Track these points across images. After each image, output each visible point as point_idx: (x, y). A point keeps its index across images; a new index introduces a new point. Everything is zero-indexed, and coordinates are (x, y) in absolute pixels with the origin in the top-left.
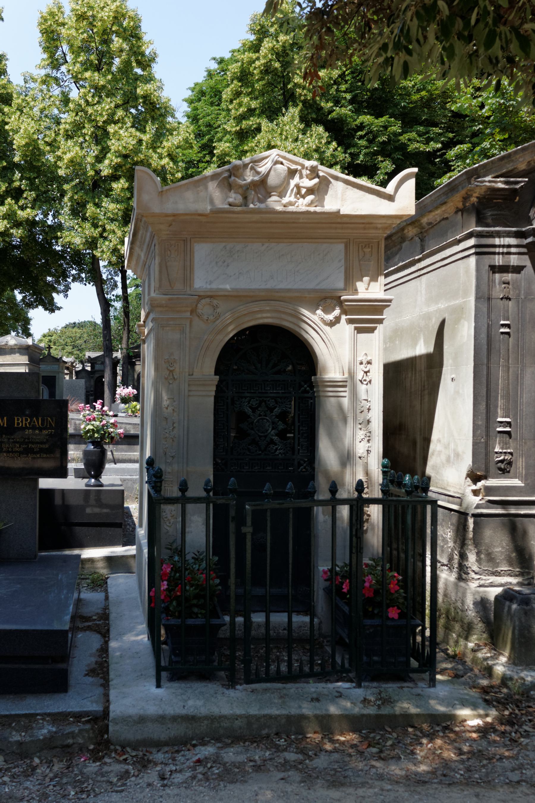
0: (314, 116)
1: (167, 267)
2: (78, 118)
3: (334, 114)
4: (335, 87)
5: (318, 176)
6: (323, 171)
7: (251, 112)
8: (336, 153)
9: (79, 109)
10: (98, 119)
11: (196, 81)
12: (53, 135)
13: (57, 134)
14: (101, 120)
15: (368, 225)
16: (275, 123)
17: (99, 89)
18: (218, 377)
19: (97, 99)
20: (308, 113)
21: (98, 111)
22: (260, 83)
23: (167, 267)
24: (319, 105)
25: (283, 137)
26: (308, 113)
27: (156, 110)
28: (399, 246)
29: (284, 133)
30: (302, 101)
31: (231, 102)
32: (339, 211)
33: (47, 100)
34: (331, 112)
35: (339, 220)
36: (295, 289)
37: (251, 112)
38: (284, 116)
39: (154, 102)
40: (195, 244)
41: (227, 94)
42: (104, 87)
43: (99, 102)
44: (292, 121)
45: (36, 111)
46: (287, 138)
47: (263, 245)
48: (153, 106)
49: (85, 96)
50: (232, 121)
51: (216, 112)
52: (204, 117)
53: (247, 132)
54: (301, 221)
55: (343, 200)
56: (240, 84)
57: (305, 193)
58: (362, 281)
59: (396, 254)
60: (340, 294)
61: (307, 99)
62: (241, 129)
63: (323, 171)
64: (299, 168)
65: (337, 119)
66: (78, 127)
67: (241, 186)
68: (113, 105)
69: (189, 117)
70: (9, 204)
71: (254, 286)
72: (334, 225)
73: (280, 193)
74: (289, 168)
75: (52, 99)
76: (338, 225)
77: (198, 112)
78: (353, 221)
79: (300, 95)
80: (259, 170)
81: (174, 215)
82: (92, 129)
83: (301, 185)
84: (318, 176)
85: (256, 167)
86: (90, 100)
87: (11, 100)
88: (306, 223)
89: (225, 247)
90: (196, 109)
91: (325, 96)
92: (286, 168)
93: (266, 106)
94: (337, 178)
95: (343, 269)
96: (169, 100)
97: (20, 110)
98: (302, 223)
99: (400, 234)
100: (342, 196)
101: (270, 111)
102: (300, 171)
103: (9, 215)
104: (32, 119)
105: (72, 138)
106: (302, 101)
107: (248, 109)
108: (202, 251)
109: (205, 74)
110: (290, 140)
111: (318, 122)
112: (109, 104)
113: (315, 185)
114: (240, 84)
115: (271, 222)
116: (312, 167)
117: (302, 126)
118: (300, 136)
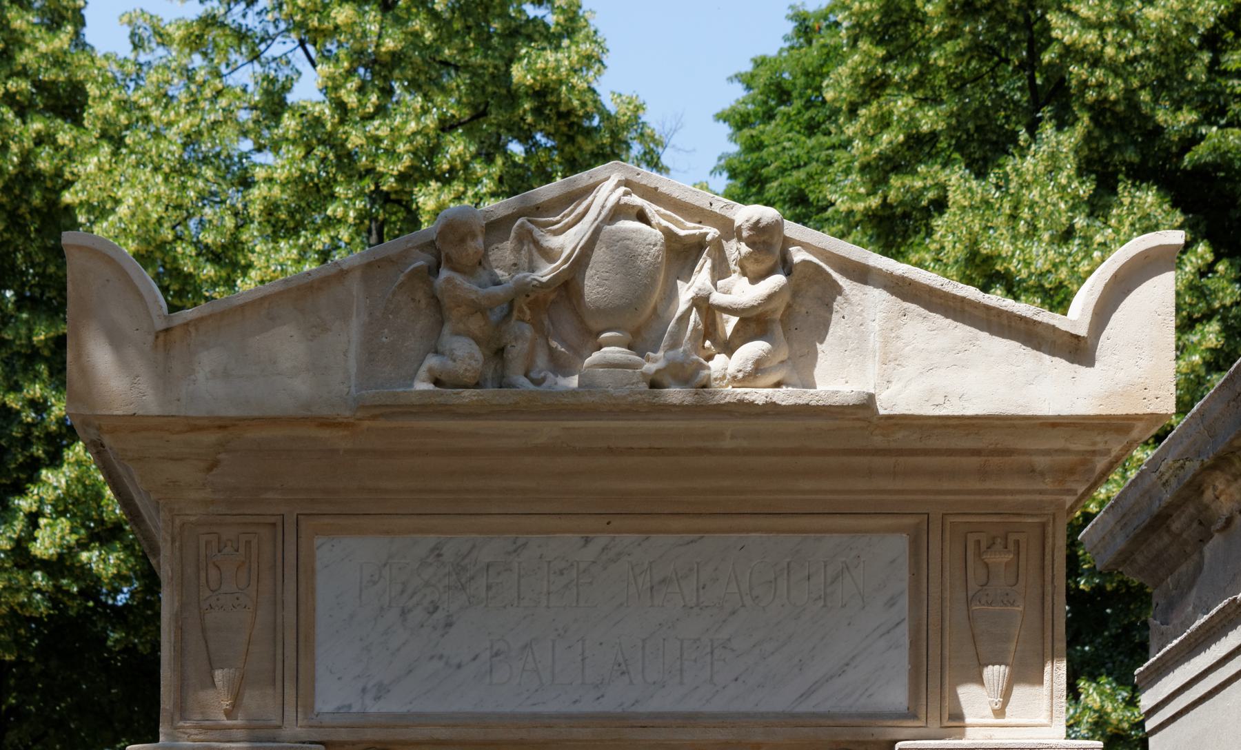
0: (1132, 156)
1: (204, 630)
2: (312, 167)
3: (1201, 152)
4: (1206, 57)
5: (786, 266)
6: (805, 246)
7: (920, 146)
8: (1211, 283)
9: (313, 133)
10: (381, 166)
11: (759, 52)
12: (230, 223)
13: (243, 220)
14: (390, 169)
15: (996, 460)
16: (992, 178)
17: (384, 65)
19: (374, 98)
20: (1112, 148)
21: (378, 140)
22: (949, 46)
23: (204, 630)
24: (1151, 118)
25: (1022, 227)
26: (1112, 148)
27: (580, 139)
28: (1196, 557)
29: (1025, 213)
30: (1090, 108)
31: (853, 112)
32: (869, 403)
33: (206, 105)
34: (1191, 140)
35: (878, 441)
36: (714, 716)
37: (920, 146)
38: (1023, 157)
39: (570, 112)
40: (318, 541)
41: (838, 86)
42: (397, 58)
43: (381, 111)
44: (1053, 169)
45: (172, 147)
46: (1032, 231)
47: (587, 541)
48: (571, 125)
49: (336, 88)
50: (855, 177)
51: (823, 154)
52: (783, 171)
53: (906, 215)
54: (728, 444)
55: (890, 359)
56: (881, 52)
57: (736, 330)
58: (979, 680)
59: (1190, 587)
60: (891, 734)
61: (1106, 99)
62: (885, 204)
63: (805, 246)
64: (712, 232)
65: (1216, 167)
66: (311, 193)
67: (478, 309)
68: (430, 121)
69: (733, 175)
70: (79, 463)
71: (554, 704)
72: (863, 461)
73: (636, 333)
74: (668, 234)
75: (223, 102)
76: (878, 461)
77: (764, 153)
78: (933, 443)
79: (1084, 85)
80: (553, 242)
81: (223, 425)
82: (359, 204)
83: (717, 298)
84: (786, 266)
85: (537, 232)
86: (352, 100)
87: (83, 105)
88: (747, 452)
89: (437, 551)
90: (755, 146)
91: (1170, 90)
92: (658, 235)
93: (971, 126)
94: (862, 274)
95: (903, 635)
96: (637, 108)
97: (110, 139)
98: (734, 452)
99: (1191, 509)
100: (886, 342)
101: (982, 143)
102: (718, 245)
103: (76, 502)
104: (156, 169)
105: (294, 232)
106: (1090, 108)
107: (908, 137)
108: (344, 566)
109: (789, 27)
110: (1046, 236)
111: (1140, 175)
112: (418, 118)
113: (771, 297)
114: (881, 52)
115: (610, 451)
116: (756, 227)
117: (1085, 189)
118: (1080, 222)
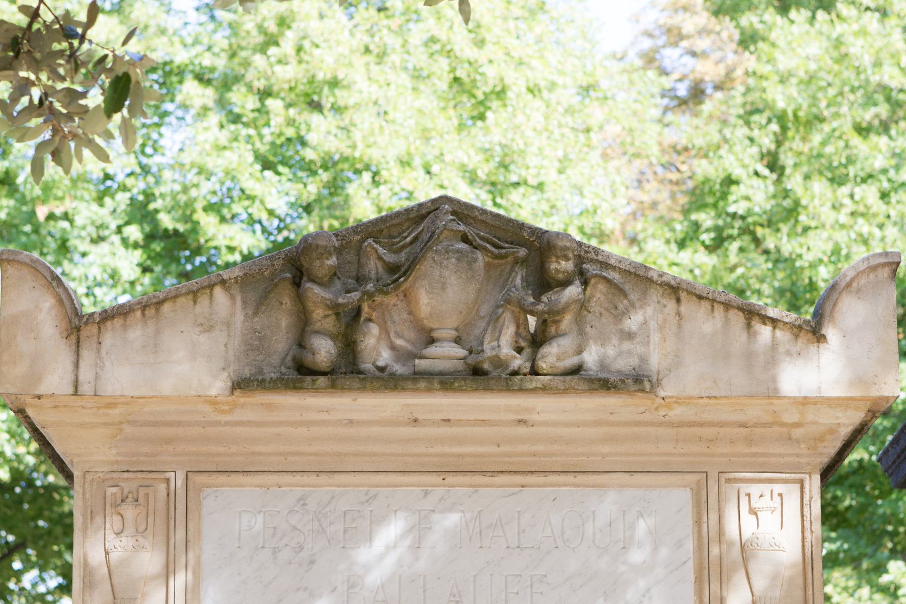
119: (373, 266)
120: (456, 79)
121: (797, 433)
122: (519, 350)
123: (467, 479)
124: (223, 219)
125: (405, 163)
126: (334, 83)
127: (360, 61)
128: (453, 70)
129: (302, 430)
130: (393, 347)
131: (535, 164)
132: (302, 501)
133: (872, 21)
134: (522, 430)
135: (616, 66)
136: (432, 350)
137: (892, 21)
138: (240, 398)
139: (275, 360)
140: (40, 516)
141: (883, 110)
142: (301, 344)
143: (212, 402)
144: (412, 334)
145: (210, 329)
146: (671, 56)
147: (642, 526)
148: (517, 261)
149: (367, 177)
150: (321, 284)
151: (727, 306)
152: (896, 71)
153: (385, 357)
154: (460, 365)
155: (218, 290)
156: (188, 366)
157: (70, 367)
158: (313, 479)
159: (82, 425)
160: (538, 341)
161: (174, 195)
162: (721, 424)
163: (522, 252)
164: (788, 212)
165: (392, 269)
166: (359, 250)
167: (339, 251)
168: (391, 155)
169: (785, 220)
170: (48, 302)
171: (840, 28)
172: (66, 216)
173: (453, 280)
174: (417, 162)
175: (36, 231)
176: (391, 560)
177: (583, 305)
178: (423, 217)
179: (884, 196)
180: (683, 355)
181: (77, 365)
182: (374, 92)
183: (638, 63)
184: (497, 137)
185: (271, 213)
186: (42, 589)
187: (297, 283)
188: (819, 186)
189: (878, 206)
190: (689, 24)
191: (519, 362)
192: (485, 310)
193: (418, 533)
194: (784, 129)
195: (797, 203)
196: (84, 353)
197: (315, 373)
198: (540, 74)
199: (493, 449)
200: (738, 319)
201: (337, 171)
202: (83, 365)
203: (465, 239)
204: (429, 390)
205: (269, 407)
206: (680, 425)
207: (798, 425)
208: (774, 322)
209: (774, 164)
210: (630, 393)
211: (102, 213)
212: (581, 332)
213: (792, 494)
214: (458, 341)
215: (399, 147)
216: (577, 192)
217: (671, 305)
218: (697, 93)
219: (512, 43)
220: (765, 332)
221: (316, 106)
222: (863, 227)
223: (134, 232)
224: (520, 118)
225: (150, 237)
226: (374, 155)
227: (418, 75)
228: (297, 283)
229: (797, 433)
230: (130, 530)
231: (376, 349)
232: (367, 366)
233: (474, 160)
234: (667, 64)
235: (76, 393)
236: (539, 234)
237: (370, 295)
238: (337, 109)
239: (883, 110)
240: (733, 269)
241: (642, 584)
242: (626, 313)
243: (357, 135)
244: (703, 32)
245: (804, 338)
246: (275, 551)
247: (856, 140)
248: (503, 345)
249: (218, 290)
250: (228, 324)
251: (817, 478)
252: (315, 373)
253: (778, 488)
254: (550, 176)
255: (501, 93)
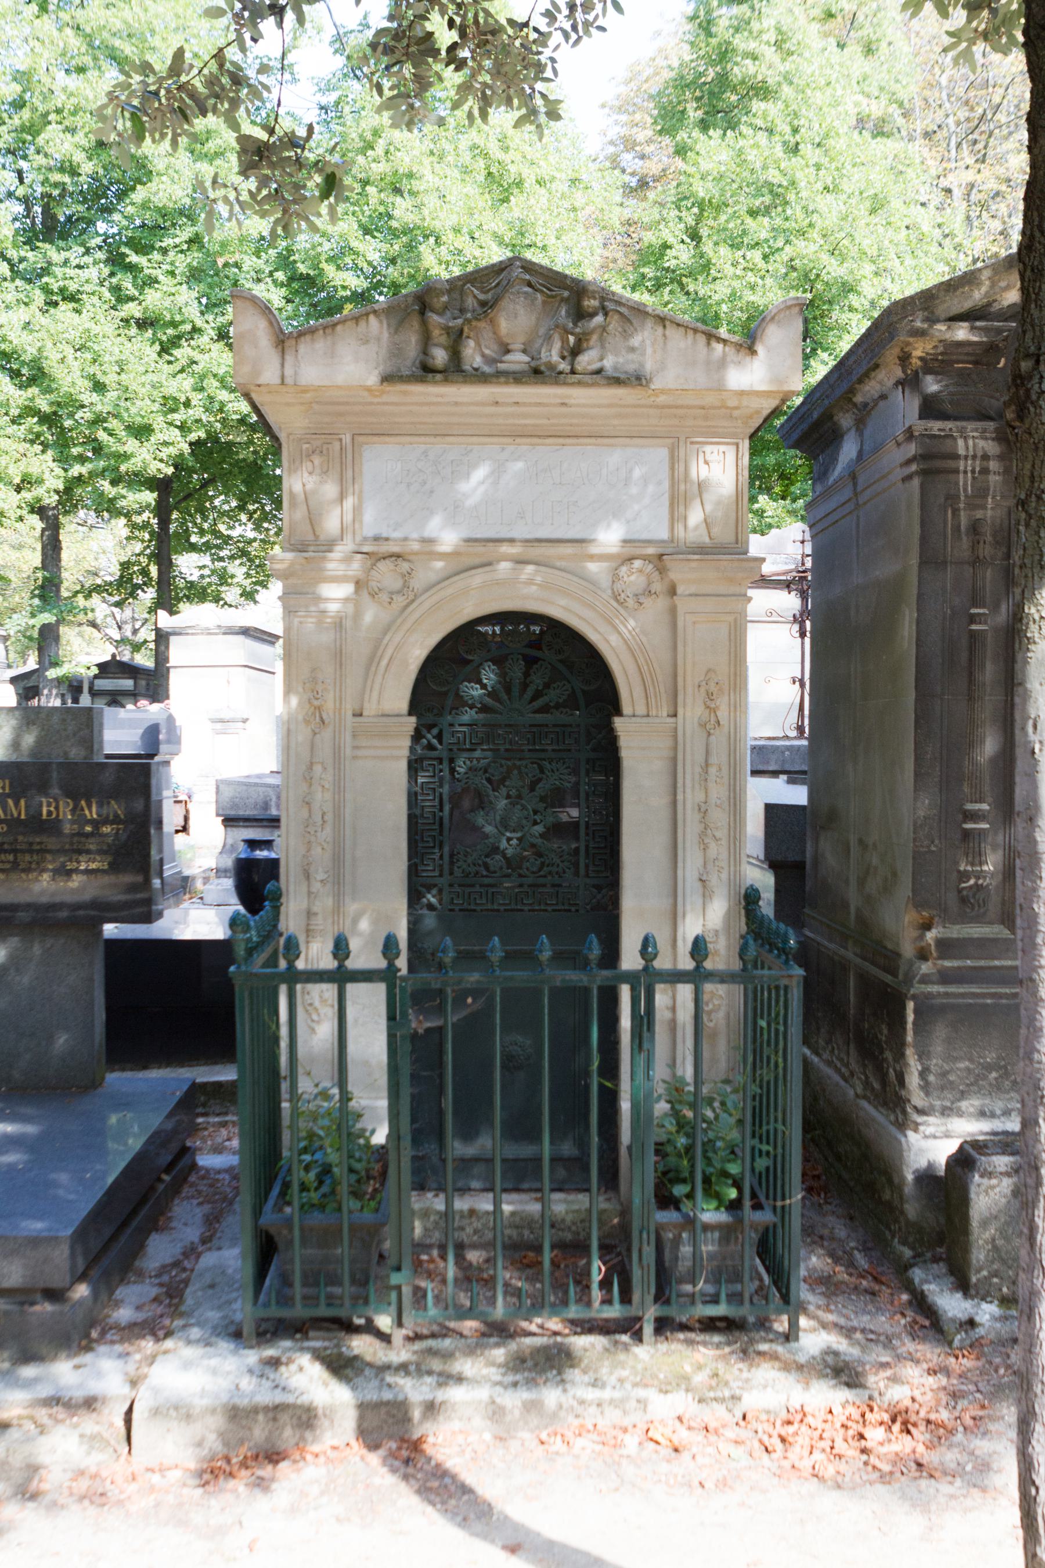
18: (413, 719)
119: (470, 302)
120: (489, 174)
121: (736, 413)
122: (563, 358)
123: (528, 440)
124: (339, 268)
125: (457, 231)
126: (410, 175)
127: (427, 161)
128: (488, 167)
129: (425, 408)
130: (483, 355)
131: (543, 232)
132: (425, 453)
133: (762, 137)
134: (564, 409)
135: (593, 166)
136: (509, 357)
137: (777, 138)
138: (387, 387)
139: (409, 363)
140: (224, 461)
141: (767, 199)
142: (425, 352)
143: (368, 389)
144: (495, 347)
145: (367, 342)
146: (628, 159)
147: (637, 473)
148: (563, 300)
149: (432, 240)
150: (440, 314)
151: (695, 331)
152: (777, 173)
153: (478, 361)
154: (526, 367)
155: (372, 317)
156: (350, 364)
157: (278, 366)
158: (432, 439)
159: (288, 404)
160: (575, 352)
161: (307, 252)
162: (689, 407)
163: (566, 294)
164: (704, 267)
165: (483, 304)
166: (462, 292)
167: (449, 292)
168: (449, 224)
169: (700, 273)
170: (262, 324)
171: (742, 142)
172: (237, 265)
173: (522, 312)
174: (465, 230)
175: (217, 274)
176: (482, 489)
177: (604, 328)
178: (503, 270)
179: (765, 257)
180: (669, 363)
181: (283, 365)
182: (437, 182)
183: (608, 164)
184: (517, 213)
185: (370, 263)
186: (226, 507)
187: (422, 313)
188: (724, 250)
189: (761, 264)
190: (642, 135)
191: (564, 366)
192: (542, 331)
193: (498, 472)
194: (702, 210)
195: (709, 261)
196: (287, 357)
197: (433, 371)
198: (545, 171)
199: (545, 421)
200: (702, 339)
201: (412, 237)
202: (287, 366)
203: (530, 285)
204: (507, 383)
205: (405, 393)
206: (663, 407)
207: (737, 408)
208: (725, 341)
209: (695, 236)
210: (633, 386)
211: (260, 263)
212: (603, 347)
213: (731, 452)
214: (524, 351)
215: (453, 220)
216: (577, 252)
217: (660, 330)
218: (643, 184)
219: (527, 149)
220: (719, 347)
221: (397, 191)
222: (751, 277)
223: (280, 276)
224: (532, 201)
225: (291, 279)
226: (437, 225)
227: (466, 171)
228: (422, 313)
229: (736, 413)
230: (318, 471)
231: (473, 355)
232: (467, 367)
233: (502, 229)
234: (623, 164)
235: (283, 383)
236: (576, 282)
237: (468, 321)
238: (411, 193)
239: (767, 199)
240: (666, 304)
241: (636, 507)
242: (631, 336)
243: (426, 212)
244: (650, 141)
245: (743, 352)
246: (409, 485)
247: (749, 220)
248: (552, 354)
249: (372, 317)
250: (379, 339)
251: (747, 442)
252: (433, 371)
253: (722, 448)
254: (551, 241)
255: (519, 184)
